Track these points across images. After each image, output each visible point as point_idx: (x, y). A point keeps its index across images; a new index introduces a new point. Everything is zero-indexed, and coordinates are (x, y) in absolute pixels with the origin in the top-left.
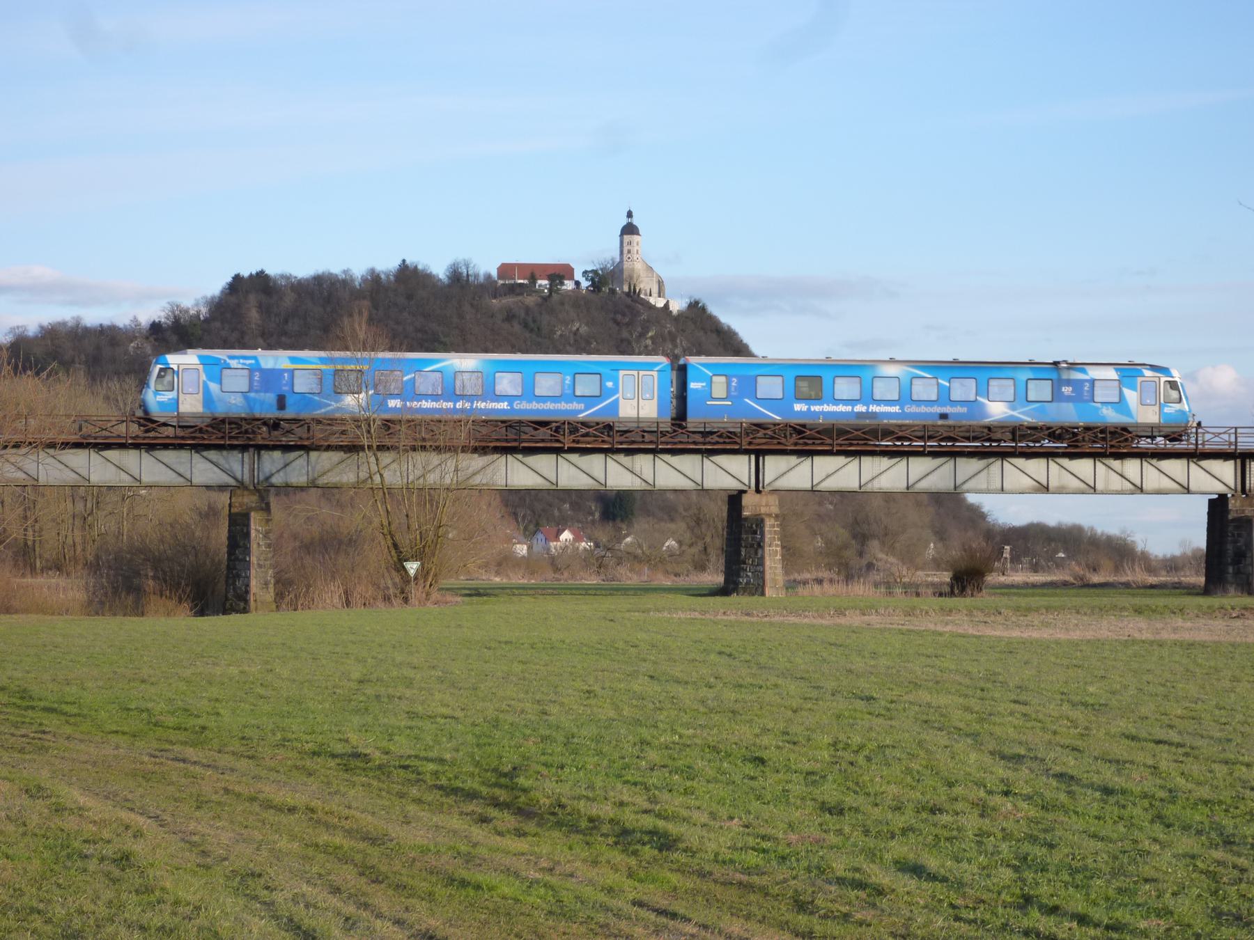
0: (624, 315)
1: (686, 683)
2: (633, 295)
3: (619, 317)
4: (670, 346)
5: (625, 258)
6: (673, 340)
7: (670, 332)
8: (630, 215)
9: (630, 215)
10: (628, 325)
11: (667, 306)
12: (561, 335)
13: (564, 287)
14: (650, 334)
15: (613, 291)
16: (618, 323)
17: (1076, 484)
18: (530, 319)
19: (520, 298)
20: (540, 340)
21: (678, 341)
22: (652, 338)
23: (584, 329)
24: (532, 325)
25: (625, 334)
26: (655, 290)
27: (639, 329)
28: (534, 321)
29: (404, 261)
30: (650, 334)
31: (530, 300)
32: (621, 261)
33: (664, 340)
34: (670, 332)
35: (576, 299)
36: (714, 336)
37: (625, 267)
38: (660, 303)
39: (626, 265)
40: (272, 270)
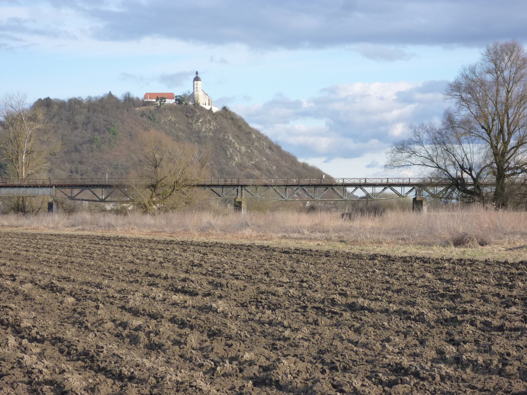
0: (190, 113)
1: (36, 284)
2: (196, 105)
3: (188, 114)
4: (208, 125)
5: (195, 90)
6: (210, 123)
7: (209, 120)
8: (197, 73)
9: (197, 73)
10: (191, 117)
11: (211, 109)
12: (164, 122)
13: (166, 102)
14: (200, 121)
15: (186, 104)
16: (187, 117)
17: (97, 199)
18: (151, 116)
19: (148, 107)
20: (154, 123)
21: (212, 123)
22: (201, 122)
23: (173, 119)
24: (152, 118)
25: (190, 121)
26: (207, 103)
27: (196, 119)
28: (153, 116)
29: (110, 92)
30: (200, 121)
31: (152, 108)
32: (194, 92)
33: (206, 123)
34: (209, 120)
35: (171, 108)
36: (230, 121)
37: (195, 94)
38: (208, 107)
39: (195, 93)
40: (52, 97)
